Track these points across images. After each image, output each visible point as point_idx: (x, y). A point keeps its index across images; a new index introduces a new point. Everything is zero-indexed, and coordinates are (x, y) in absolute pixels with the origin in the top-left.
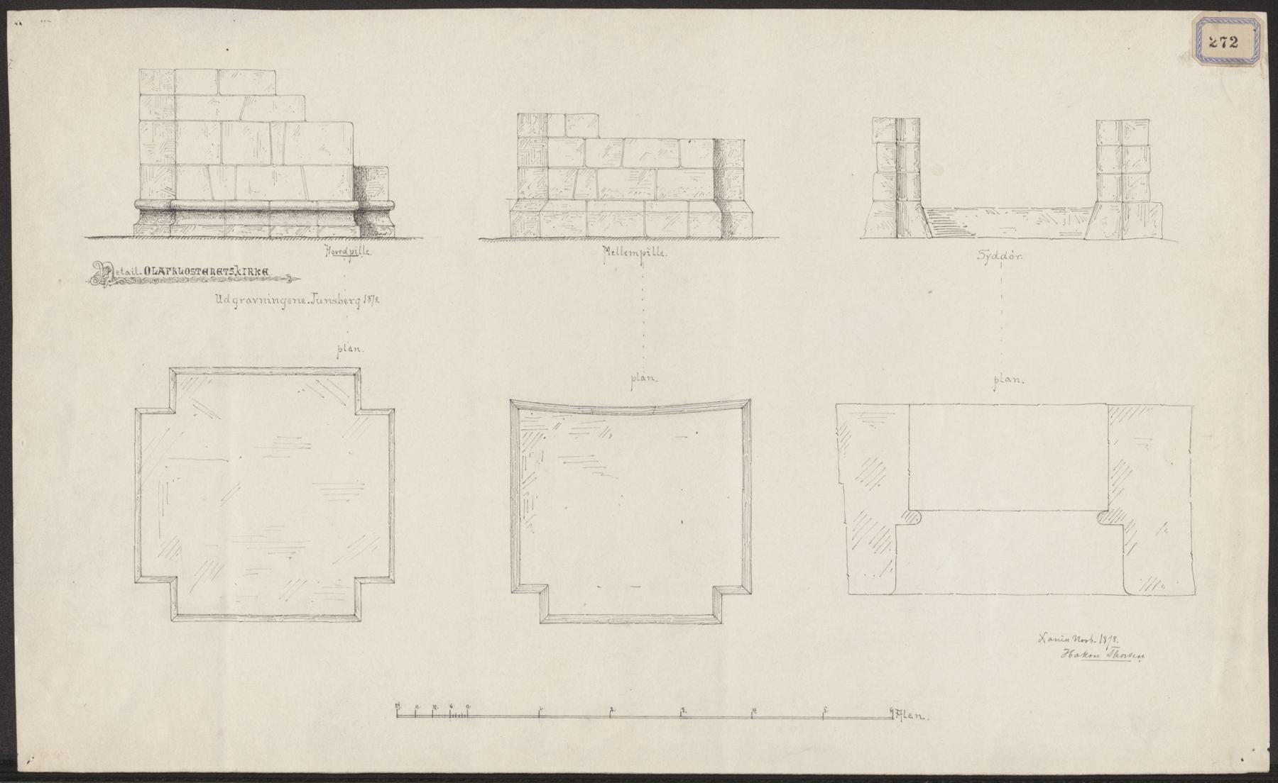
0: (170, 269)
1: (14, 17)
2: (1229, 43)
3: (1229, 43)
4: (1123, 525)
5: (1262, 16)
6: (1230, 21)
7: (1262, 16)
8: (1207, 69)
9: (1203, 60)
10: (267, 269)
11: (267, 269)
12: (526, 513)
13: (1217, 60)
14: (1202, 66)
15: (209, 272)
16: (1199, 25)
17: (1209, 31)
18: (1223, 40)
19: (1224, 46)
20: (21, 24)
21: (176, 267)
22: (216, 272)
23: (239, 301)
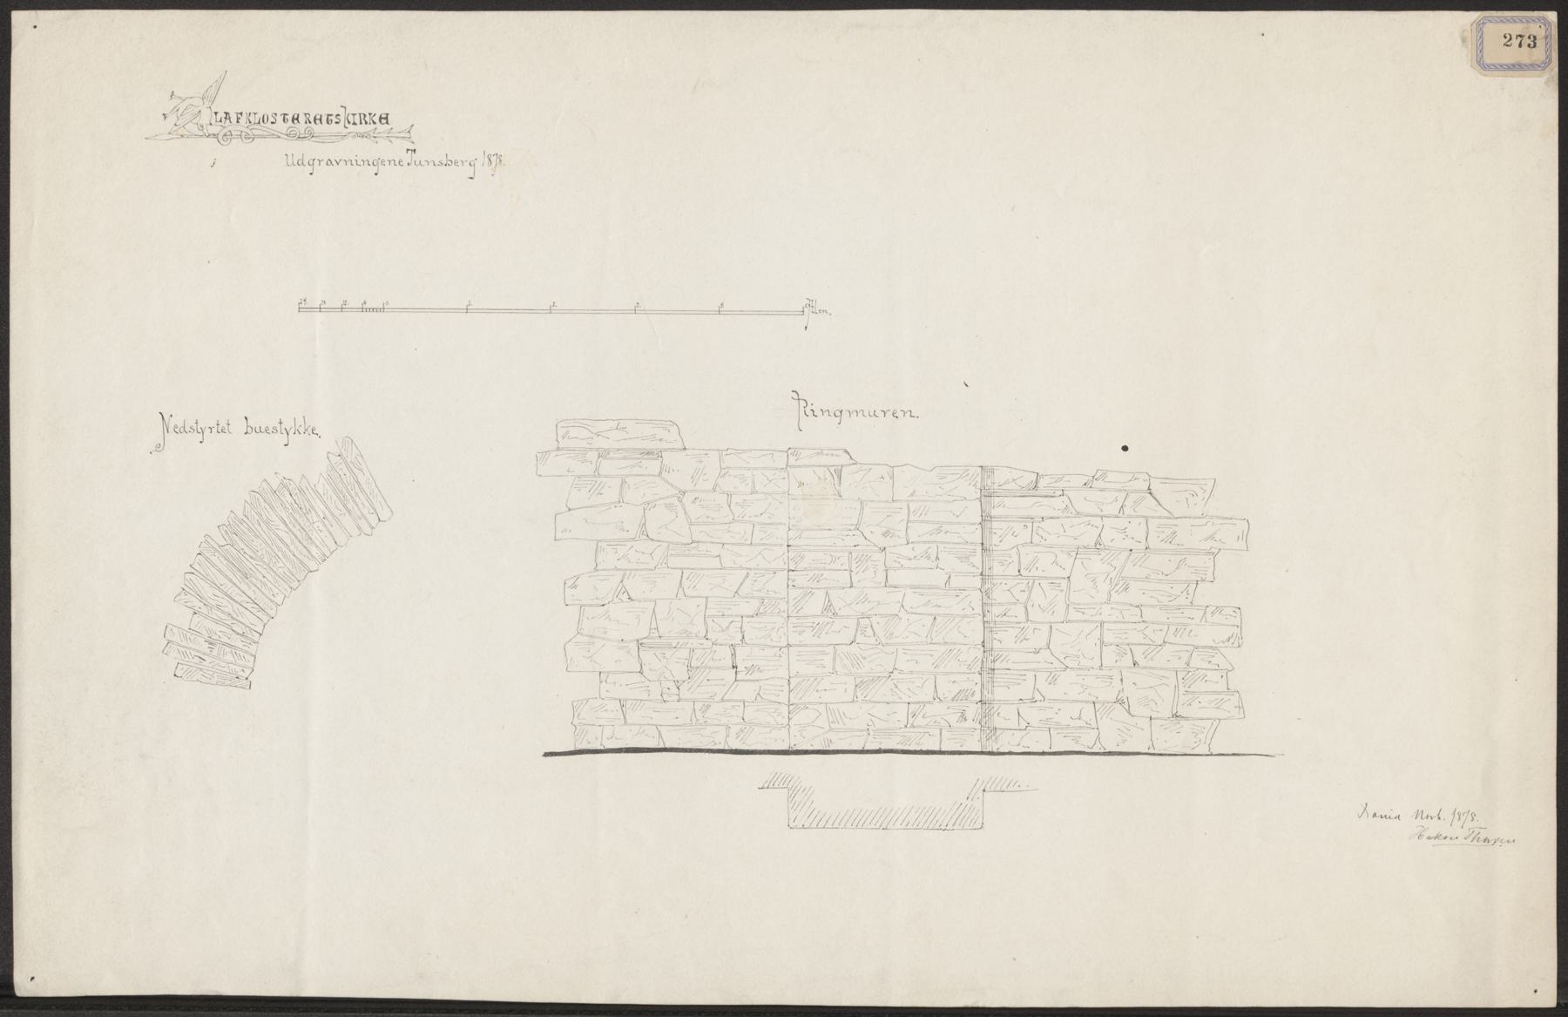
0: (241, 114)
1: (1547, 997)
2: (1526, 41)
3: (1526, 41)
4: (911, 416)
5: (1552, 16)
6: (1507, 20)
7: (1552, 16)
8: (1493, 81)
9: (1484, 66)
10: (387, 114)
11: (387, 114)
12: (1063, 735)
13: (1501, 66)
14: (1485, 76)
15: (302, 119)
16: (1480, 25)
17: (1490, 29)
18: (1519, 39)
19: (1520, 45)
20: (1547, 997)
21: (353, 159)
22: (312, 120)
23: (316, 162)
